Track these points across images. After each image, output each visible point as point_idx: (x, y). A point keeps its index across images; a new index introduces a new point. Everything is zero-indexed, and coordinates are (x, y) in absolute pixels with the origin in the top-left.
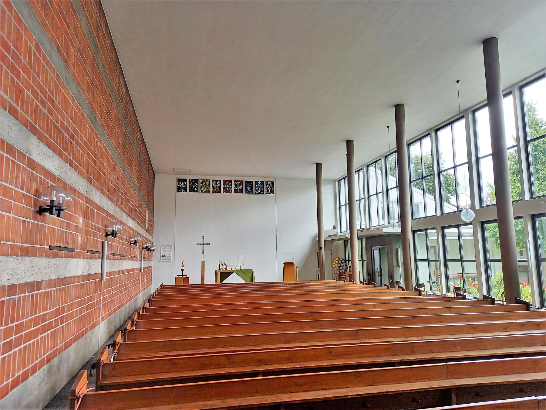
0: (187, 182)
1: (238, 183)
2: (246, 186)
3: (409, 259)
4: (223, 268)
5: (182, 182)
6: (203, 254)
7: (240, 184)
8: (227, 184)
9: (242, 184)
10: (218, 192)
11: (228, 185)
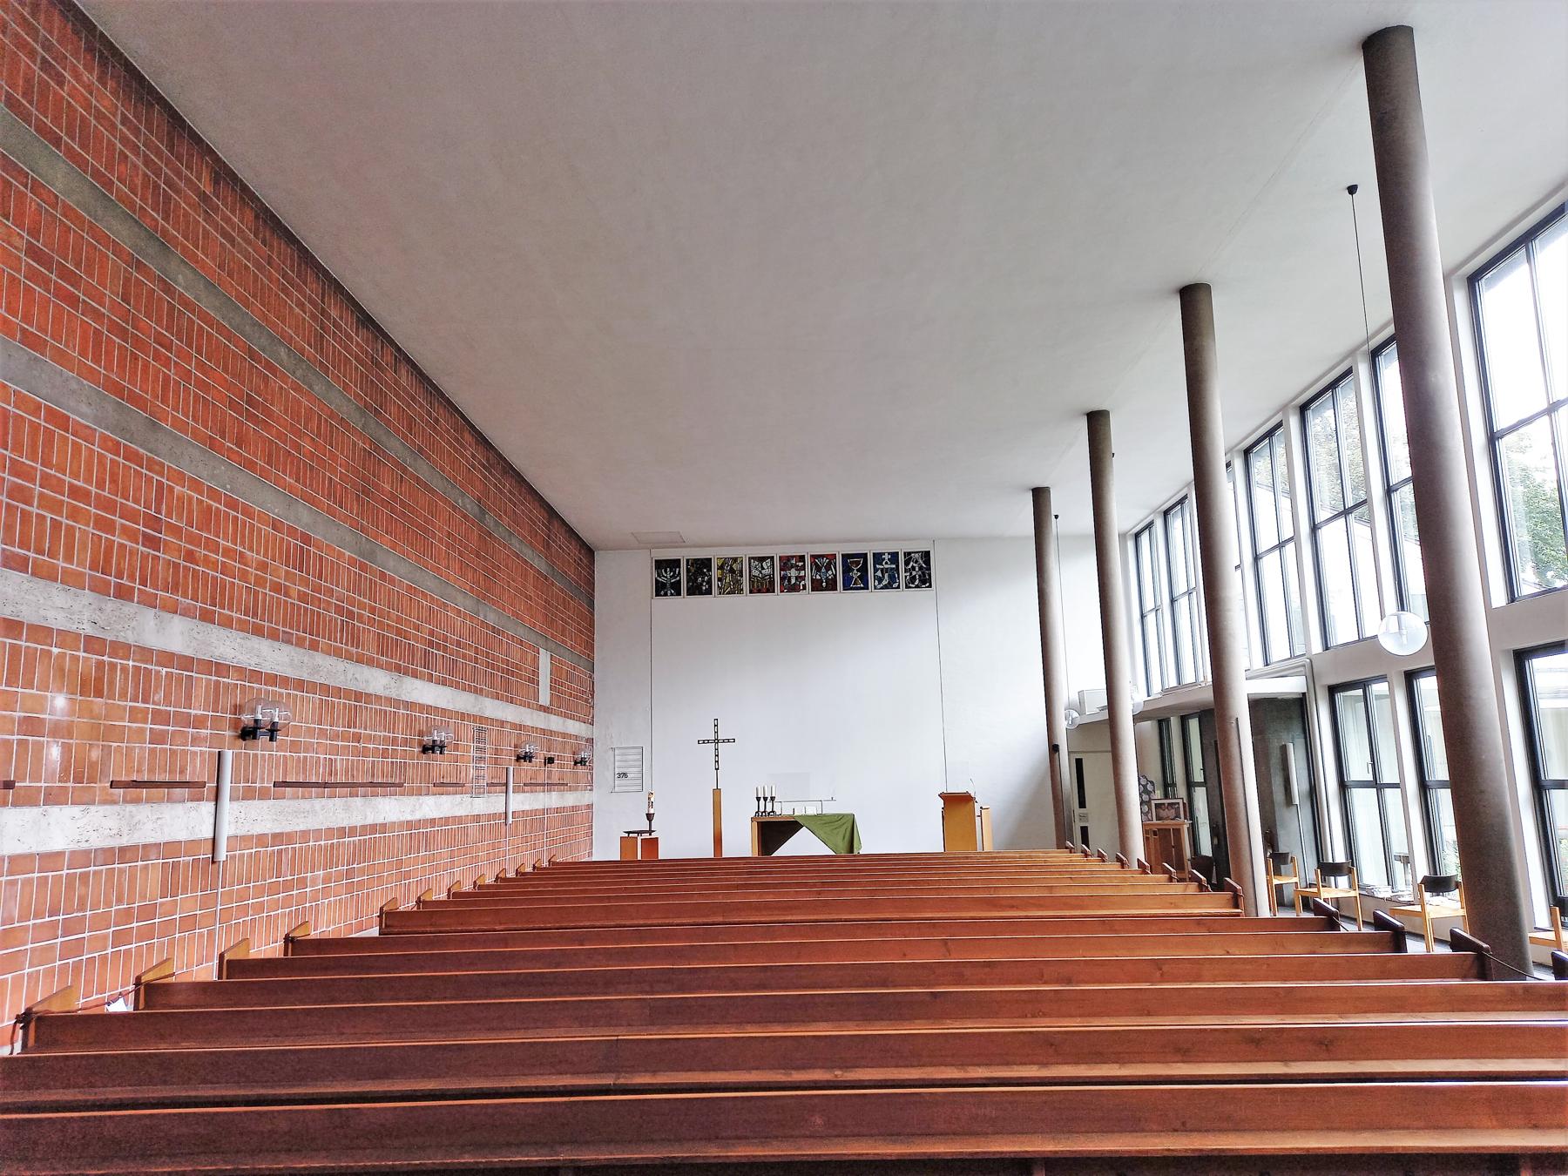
0: (680, 568)
1: (822, 562)
2: (847, 570)
3: (1238, 782)
4: (769, 809)
5: (668, 569)
6: (717, 769)
7: (829, 563)
8: (792, 567)
9: (835, 564)
10: (768, 591)
11: (793, 570)
